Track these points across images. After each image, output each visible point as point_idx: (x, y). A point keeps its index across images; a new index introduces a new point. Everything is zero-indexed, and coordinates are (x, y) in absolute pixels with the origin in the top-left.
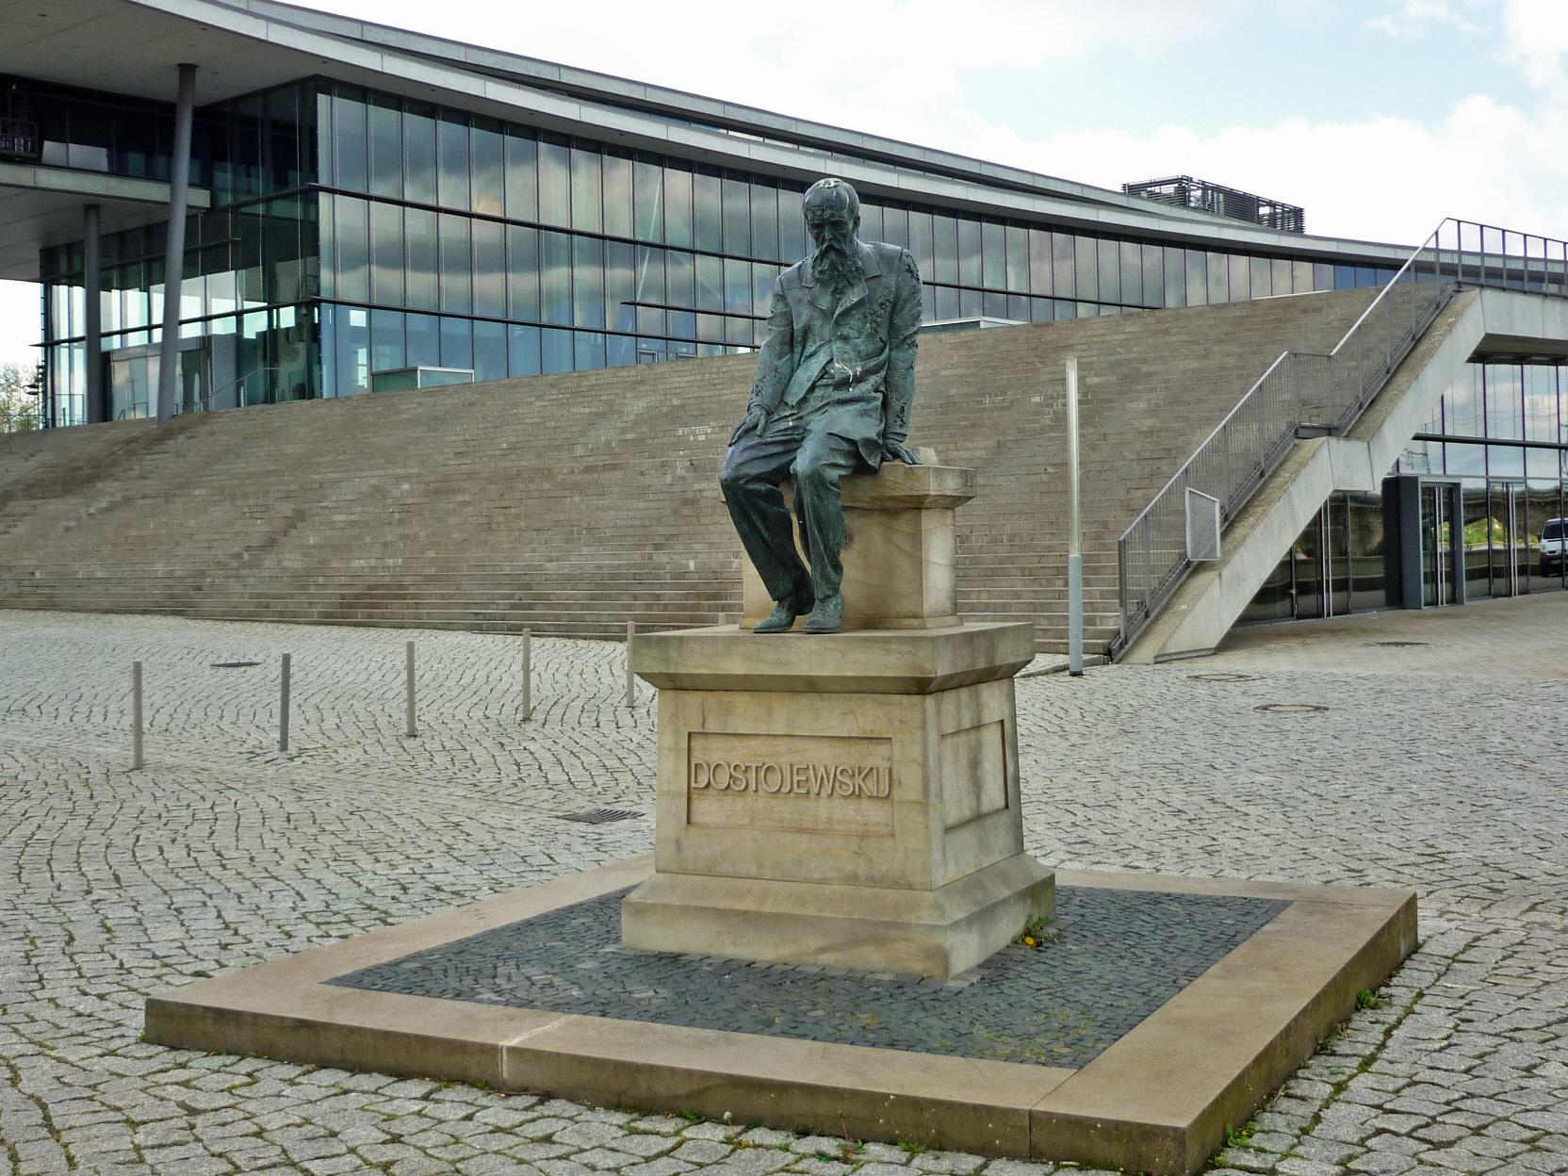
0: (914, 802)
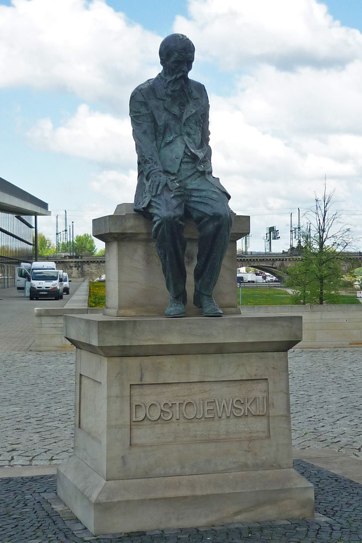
0: (282, 416)
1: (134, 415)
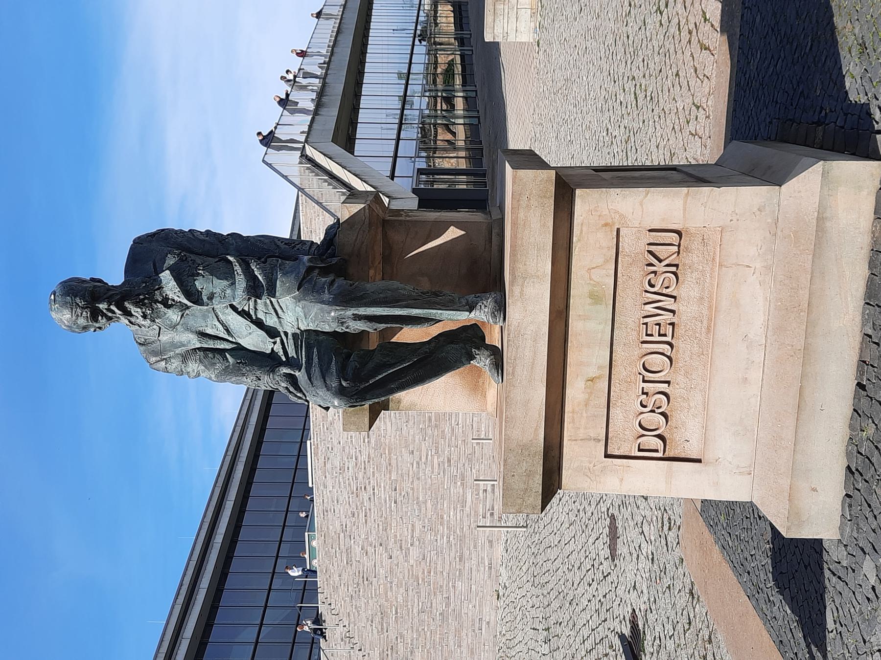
0: (685, 203)
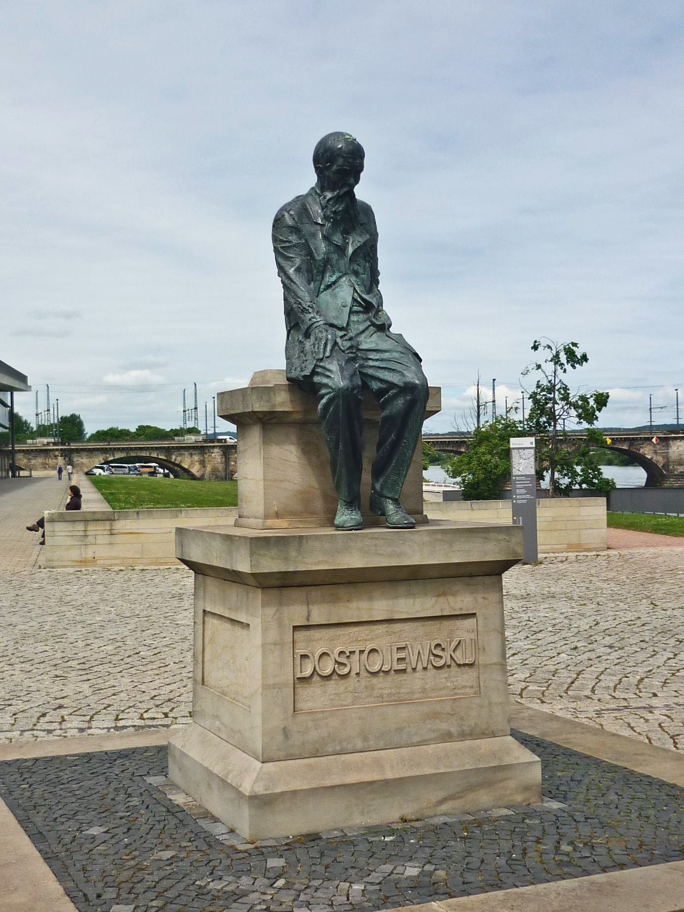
0: (495, 664)
1: (299, 670)
